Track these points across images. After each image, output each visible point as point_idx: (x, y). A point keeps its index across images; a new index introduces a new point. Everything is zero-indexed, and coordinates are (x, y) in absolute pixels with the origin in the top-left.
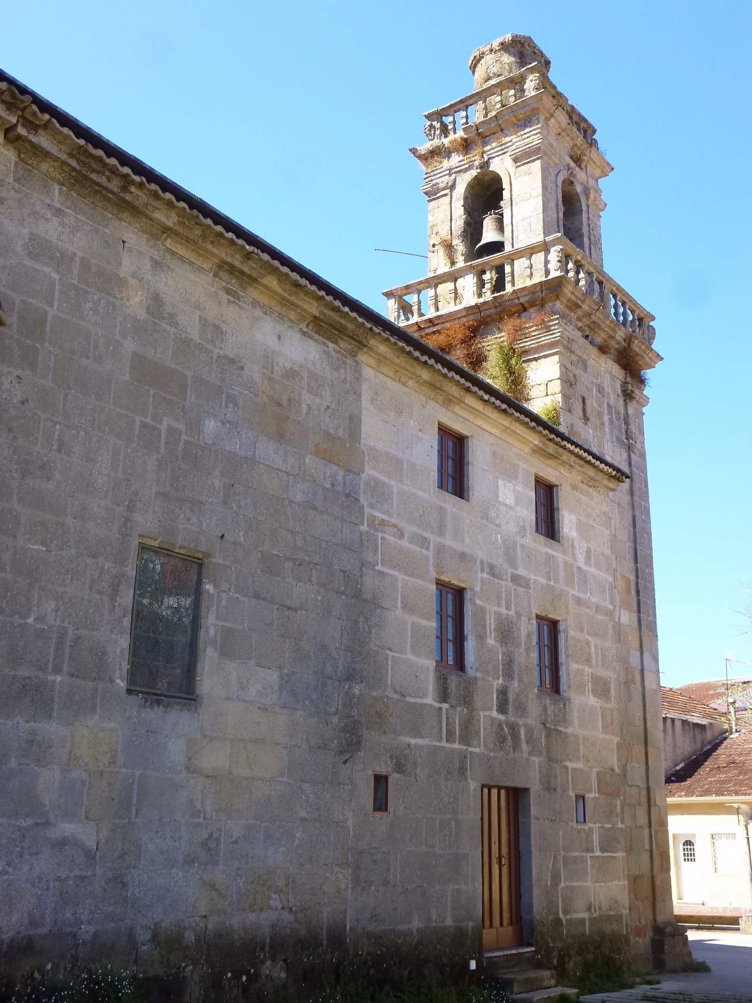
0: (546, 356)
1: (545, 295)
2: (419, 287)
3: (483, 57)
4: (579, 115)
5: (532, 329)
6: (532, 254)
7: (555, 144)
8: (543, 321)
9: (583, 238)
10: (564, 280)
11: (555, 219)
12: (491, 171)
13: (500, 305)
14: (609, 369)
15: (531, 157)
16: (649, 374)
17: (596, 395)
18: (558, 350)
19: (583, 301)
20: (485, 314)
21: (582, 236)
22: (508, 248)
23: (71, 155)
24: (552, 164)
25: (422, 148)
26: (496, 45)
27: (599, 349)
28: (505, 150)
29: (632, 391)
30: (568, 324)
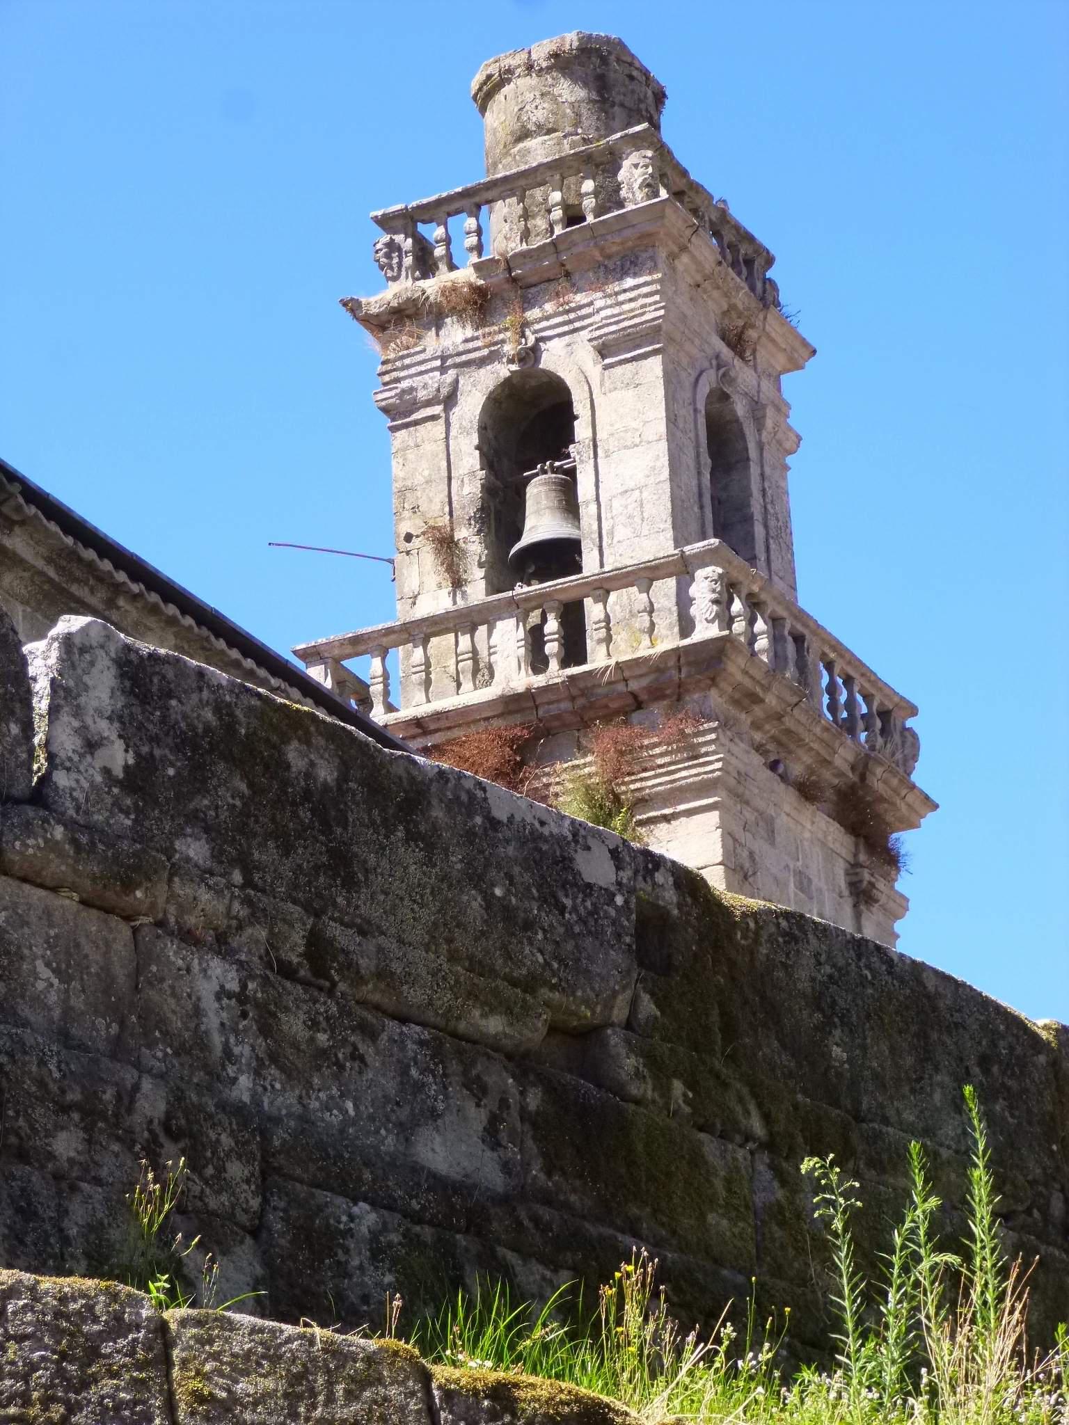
0: (689, 813)
1: (689, 676)
2: (385, 641)
3: (509, 81)
4: (737, 228)
5: (657, 751)
6: (652, 580)
7: (689, 313)
8: (682, 732)
9: (752, 525)
10: (728, 645)
11: (695, 489)
12: (544, 371)
13: (583, 695)
14: (820, 836)
15: (639, 347)
16: (907, 841)
17: (796, 895)
18: (716, 799)
19: (766, 689)
20: (548, 711)
21: (749, 519)
22: (590, 563)
23: (49, 560)
24: (685, 361)
25: (372, 299)
26: (541, 52)
27: (799, 790)
28: (577, 325)
29: (872, 885)
30: (736, 740)
